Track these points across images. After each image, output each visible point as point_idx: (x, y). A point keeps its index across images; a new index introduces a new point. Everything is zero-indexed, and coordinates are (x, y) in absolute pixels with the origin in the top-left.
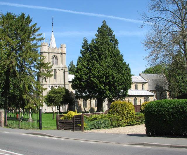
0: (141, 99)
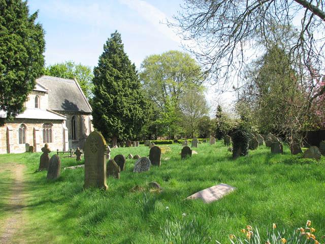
0: (36, 129)
